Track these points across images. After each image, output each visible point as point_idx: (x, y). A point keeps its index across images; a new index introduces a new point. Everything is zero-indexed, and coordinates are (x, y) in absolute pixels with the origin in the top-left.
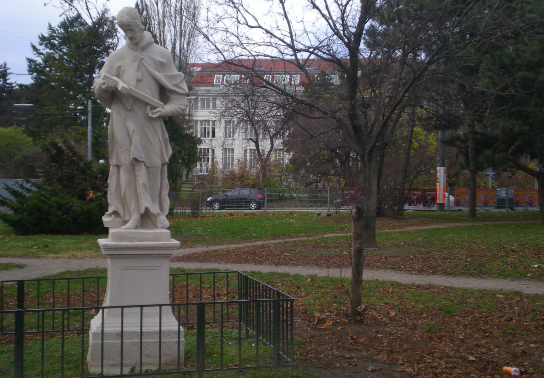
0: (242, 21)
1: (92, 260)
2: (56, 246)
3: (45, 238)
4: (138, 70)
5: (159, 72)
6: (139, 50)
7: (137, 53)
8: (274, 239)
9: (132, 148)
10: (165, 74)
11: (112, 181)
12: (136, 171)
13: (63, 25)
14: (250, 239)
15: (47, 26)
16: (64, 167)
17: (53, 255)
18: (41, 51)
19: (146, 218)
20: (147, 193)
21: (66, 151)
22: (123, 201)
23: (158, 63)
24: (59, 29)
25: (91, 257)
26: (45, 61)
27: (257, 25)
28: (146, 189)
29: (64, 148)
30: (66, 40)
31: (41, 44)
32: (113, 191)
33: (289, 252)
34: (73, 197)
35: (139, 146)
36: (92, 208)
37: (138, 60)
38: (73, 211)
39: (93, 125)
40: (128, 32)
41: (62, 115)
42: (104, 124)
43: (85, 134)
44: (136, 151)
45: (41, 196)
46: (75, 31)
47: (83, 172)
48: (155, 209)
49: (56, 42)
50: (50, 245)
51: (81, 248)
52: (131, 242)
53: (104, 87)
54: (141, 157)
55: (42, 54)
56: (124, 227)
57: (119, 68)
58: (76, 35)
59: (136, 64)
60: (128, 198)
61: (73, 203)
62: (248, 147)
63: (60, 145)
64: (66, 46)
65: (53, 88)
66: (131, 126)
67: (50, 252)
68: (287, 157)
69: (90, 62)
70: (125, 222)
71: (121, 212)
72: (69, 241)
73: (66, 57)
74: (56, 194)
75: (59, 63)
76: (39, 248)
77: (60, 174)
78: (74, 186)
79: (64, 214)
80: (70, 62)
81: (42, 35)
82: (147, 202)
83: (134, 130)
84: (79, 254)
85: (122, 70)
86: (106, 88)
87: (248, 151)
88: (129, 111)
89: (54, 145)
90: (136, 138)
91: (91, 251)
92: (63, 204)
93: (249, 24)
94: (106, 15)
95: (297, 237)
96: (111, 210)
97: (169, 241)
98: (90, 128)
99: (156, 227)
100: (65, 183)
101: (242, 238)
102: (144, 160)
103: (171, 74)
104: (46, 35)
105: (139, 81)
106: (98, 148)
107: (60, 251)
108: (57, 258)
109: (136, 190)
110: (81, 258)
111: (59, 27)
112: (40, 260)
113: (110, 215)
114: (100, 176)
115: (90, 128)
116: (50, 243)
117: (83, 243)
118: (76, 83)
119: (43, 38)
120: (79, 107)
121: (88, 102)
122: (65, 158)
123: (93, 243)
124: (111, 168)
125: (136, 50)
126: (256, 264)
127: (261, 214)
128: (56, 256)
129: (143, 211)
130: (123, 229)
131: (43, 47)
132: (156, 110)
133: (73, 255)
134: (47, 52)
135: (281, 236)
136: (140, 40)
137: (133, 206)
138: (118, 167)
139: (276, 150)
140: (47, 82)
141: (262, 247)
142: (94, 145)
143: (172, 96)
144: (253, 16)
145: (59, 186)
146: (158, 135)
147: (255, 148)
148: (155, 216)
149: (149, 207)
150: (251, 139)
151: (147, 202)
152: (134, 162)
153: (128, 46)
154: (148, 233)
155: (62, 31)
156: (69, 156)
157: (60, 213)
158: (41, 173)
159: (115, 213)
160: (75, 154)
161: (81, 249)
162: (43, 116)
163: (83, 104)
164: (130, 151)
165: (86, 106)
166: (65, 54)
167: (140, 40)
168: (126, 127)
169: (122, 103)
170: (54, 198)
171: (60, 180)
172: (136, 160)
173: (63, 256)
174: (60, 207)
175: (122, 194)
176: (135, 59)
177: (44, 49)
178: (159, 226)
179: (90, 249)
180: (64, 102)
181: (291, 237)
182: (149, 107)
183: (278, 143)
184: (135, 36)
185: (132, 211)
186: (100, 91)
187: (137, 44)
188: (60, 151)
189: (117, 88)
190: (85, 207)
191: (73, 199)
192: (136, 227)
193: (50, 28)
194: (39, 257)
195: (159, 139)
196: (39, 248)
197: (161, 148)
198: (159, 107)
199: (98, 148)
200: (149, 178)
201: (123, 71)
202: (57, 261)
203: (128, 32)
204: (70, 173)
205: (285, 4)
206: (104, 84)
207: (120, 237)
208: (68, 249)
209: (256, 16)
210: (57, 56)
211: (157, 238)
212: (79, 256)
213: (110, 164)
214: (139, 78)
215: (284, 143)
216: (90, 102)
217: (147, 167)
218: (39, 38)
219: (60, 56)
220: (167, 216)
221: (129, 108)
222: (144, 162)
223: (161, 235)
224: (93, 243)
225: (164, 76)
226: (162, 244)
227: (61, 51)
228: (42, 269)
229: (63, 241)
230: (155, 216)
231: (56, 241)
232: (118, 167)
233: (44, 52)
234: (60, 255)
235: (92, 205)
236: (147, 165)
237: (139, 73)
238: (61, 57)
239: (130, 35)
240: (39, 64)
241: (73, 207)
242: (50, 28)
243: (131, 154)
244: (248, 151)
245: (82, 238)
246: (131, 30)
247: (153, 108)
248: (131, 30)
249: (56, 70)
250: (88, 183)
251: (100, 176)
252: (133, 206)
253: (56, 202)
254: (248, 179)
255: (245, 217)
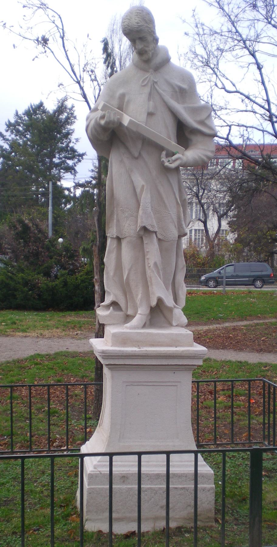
0: (220, 85)
1: (60, 340)
2: (23, 323)
3: (12, 314)
4: (149, 100)
5: (178, 103)
6: (151, 70)
7: (147, 75)
8: (242, 320)
9: (141, 212)
10: (186, 105)
11: (109, 259)
12: (145, 246)
13: (28, 113)
14: (217, 320)
15: (14, 112)
16: (30, 244)
17: (21, 334)
18: (7, 137)
19: (158, 313)
20: (160, 278)
21: (32, 229)
22: (126, 288)
23: (177, 90)
24: (23, 116)
25: (59, 337)
26: (11, 147)
27: (235, 90)
28: (158, 273)
29: (31, 225)
30: (28, 127)
31: (7, 131)
32: (111, 274)
33: (267, 336)
34: (39, 273)
35: (150, 210)
36: (57, 285)
37: (150, 85)
38: (39, 288)
39: (53, 206)
40: (138, 42)
41: (25, 195)
42: (63, 205)
43: (46, 214)
44: (145, 218)
45: (8, 272)
46: (38, 118)
47: (48, 249)
48: (169, 301)
49: (21, 129)
50: (17, 322)
51: (48, 326)
52: (139, 346)
53: (103, 122)
54: (153, 226)
55: (8, 140)
56: (128, 325)
57: (123, 96)
58: (39, 122)
59: (147, 90)
60: (133, 284)
61: (38, 280)
62: (193, 228)
63: (27, 221)
64: (30, 132)
65: (17, 171)
66: (139, 181)
67: (17, 330)
68: (231, 237)
69: (51, 147)
70: (128, 318)
71: (122, 304)
72: (36, 317)
73: (29, 143)
74: (22, 271)
75: (23, 148)
76: (6, 325)
77: (26, 250)
78: (39, 263)
79: (30, 290)
80: (33, 147)
81: (9, 121)
82: (160, 291)
83: (143, 186)
84: (46, 333)
85: (126, 99)
86: (107, 123)
87: (193, 232)
88: (136, 158)
89: (21, 221)
90: (146, 198)
91: (58, 331)
92: (29, 280)
93: (227, 88)
94: (66, 103)
95: (265, 318)
96: (108, 300)
97: (192, 346)
98: (50, 208)
99: (171, 325)
100: (31, 259)
101: (209, 319)
102: (156, 229)
103: (196, 105)
104: (13, 121)
105: (150, 114)
106: (57, 228)
107: (28, 329)
108: (26, 337)
109: (144, 273)
110: (50, 338)
111: (24, 114)
112: (8, 338)
113: (108, 307)
114: (64, 253)
115: (50, 208)
116: (17, 320)
117: (50, 320)
118: (38, 166)
119: (9, 125)
120: (40, 189)
121: (48, 184)
122: (31, 235)
123: (59, 321)
124: (109, 241)
125: (146, 70)
126: (236, 350)
127: (220, 293)
128: (25, 334)
129: (154, 303)
130: (127, 328)
131: (9, 133)
132: (174, 158)
133: (41, 334)
134: (12, 138)
135: (248, 317)
136: (153, 54)
137: (140, 296)
138: (119, 239)
139: (223, 230)
140: (14, 165)
141: (234, 329)
142: (54, 225)
143: (195, 139)
144: (231, 82)
145: (26, 263)
146: (174, 194)
147: (204, 228)
148: (171, 310)
149: (163, 297)
150: (200, 220)
151: (160, 291)
152: (142, 233)
153: (136, 65)
154: (163, 334)
155: (26, 118)
156: (34, 233)
157: (26, 289)
158: (9, 249)
159: (114, 304)
160: (40, 231)
161: (47, 327)
162: (9, 197)
163: (44, 187)
164: (137, 217)
165: (47, 189)
166: (28, 140)
167: (153, 54)
168: (132, 182)
169: (127, 148)
170: (21, 275)
171: (27, 258)
172: (145, 229)
173: (31, 334)
174: (26, 283)
175: (125, 278)
176: (145, 83)
177: (10, 136)
178: (174, 324)
179: (57, 328)
180: (27, 184)
181: (259, 318)
182: (164, 153)
183: (224, 224)
184: (147, 49)
185: (138, 302)
186: (95, 129)
187: (147, 61)
188: (26, 228)
189: (121, 124)
190: (50, 284)
191: (39, 276)
192: (144, 326)
193: (17, 114)
194: (8, 336)
195: (176, 199)
196: (6, 325)
197: (178, 212)
198: (178, 152)
199: (57, 228)
200: (162, 258)
201: (128, 102)
202: (25, 340)
203: (138, 42)
204: (36, 250)
205: (263, 70)
206: (103, 117)
207: (123, 340)
208: (35, 326)
209: (234, 82)
210: (21, 142)
211: (175, 342)
212: (47, 336)
213: (108, 235)
214: (151, 110)
215: (230, 224)
216: (51, 183)
217: (159, 240)
218: (6, 124)
219: (24, 142)
220: (184, 310)
221: (136, 154)
222: (156, 232)
223: (179, 338)
224: (59, 321)
225: (185, 108)
226: (183, 351)
227: (25, 137)
228: (11, 350)
229: (29, 318)
230: (171, 310)
231: (23, 318)
232: (119, 239)
233: (10, 138)
234: (28, 334)
235: (57, 282)
236: (159, 237)
237: (151, 103)
238: (25, 143)
239: (140, 46)
240: (5, 150)
241: (38, 284)
242: (17, 114)
243: (139, 221)
244: (193, 232)
245: (47, 315)
246: (142, 39)
247: (170, 154)
248: (142, 39)
249: (20, 154)
250: (53, 260)
251: (64, 253)
252: (139, 296)
253: (23, 279)
254: (199, 258)
255: (204, 296)
